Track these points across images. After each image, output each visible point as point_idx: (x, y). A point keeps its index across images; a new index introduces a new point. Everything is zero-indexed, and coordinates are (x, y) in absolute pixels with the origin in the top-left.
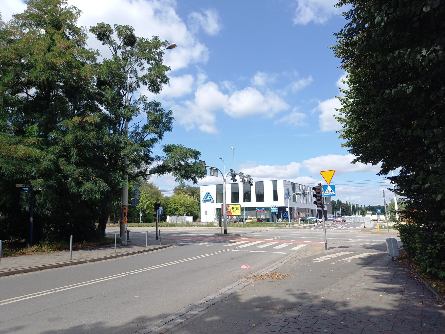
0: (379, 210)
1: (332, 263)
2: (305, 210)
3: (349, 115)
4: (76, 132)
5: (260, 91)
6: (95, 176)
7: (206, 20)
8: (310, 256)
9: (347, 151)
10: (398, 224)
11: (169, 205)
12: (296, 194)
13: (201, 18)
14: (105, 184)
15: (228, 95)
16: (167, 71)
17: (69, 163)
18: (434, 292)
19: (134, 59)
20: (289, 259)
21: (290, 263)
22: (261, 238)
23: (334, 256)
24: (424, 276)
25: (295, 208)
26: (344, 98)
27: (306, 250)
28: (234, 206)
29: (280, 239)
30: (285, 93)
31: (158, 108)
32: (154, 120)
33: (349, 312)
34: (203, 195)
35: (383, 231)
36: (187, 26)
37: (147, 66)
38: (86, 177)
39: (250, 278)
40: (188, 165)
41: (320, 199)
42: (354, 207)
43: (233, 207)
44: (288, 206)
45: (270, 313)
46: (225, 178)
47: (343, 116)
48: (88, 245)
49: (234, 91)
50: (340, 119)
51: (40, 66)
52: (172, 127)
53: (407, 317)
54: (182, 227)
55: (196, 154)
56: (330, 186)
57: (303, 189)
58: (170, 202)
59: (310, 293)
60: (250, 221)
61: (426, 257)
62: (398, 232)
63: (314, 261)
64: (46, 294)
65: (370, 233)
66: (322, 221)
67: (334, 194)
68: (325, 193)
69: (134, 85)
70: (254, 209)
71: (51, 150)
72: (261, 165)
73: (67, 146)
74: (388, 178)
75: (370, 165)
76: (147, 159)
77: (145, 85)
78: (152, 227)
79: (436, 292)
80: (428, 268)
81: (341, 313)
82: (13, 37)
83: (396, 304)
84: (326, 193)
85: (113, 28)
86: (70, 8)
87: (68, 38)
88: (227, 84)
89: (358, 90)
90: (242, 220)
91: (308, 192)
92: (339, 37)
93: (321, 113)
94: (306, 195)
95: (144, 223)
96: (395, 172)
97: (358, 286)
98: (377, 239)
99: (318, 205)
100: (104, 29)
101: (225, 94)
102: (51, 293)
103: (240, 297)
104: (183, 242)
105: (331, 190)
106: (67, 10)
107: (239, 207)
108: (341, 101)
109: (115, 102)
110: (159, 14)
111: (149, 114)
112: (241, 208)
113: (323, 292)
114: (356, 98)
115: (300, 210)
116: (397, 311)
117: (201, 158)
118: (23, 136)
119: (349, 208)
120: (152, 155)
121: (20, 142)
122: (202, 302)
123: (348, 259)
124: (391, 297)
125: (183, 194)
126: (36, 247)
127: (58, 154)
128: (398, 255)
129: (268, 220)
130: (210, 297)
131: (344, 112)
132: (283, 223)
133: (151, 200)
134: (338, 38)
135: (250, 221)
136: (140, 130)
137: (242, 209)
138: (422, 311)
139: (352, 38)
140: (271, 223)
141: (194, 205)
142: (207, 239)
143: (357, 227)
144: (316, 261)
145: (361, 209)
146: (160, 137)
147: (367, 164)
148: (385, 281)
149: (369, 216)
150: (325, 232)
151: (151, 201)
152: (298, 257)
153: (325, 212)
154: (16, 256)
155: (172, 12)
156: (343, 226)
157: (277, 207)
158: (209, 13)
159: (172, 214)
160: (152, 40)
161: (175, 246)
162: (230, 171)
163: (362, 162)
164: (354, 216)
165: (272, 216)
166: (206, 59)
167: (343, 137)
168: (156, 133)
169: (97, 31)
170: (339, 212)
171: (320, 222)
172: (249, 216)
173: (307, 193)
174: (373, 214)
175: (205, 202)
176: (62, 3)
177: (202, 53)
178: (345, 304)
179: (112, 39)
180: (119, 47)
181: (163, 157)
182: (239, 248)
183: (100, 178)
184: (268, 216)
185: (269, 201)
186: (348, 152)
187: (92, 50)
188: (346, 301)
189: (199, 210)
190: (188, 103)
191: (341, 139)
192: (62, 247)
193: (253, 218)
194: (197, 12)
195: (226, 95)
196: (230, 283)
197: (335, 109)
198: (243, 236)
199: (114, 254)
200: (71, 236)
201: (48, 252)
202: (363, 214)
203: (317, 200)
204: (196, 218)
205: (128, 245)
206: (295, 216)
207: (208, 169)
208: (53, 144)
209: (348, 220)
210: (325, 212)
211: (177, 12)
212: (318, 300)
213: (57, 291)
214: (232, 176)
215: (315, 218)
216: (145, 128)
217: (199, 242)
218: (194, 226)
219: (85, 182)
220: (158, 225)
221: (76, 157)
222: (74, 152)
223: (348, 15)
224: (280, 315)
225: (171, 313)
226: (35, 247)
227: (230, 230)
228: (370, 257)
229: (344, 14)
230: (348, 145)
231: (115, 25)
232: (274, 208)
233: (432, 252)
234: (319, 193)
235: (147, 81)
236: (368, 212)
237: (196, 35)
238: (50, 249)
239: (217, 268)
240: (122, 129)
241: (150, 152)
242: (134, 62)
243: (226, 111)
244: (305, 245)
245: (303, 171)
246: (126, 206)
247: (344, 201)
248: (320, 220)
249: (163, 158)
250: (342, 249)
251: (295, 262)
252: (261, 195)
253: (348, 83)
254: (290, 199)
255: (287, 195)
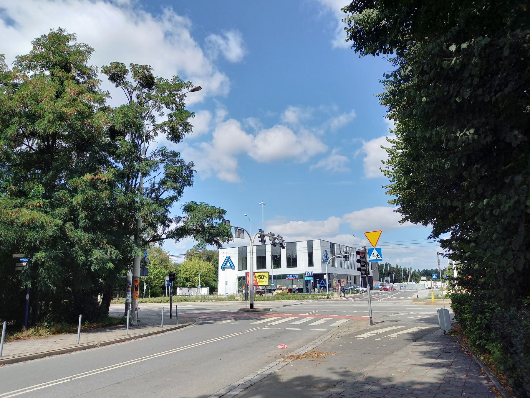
0: (434, 276)
1: (377, 339)
2: (347, 277)
3: (397, 168)
4: (87, 192)
5: (292, 129)
6: (105, 242)
7: (227, 44)
8: (352, 332)
9: (394, 211)
10: (450, 292)
11: (179, 273)
12: (336, 257)
13: (221, 41)
14: (117, 251)
15: (253, 134)
16: (190, 117)
17: (77, 228)
18: (480, 365)
19: (151, 103)
20: (329, 337)
21: (331, 341)
22: (294, 313)
23: (380, 331)
24: (474, 350)
25: (335, 275)
26: (392, 148)
27: (349, 326)
28: (261, 274)
29: (317, 313)
30: (322, 132)
31: (177, 159)
32: (172, 174)
33: (393, 386)
34: (221, 261)
35: (439, 301)
36: (204, 52)
37: (166, 111)
38: (95, 244)
39: (288, 357)
40: (212, 227)
41: (365, 265)
42: (405, 272)
43: (259, 275)
44: (327, 273)
45: (313, 391)
46: (253, 240)
47: (390, 170)
48: (91, 327)
49: (260, 130)
50: (387, 173)
51: (49, 116)
52: (193, 182)
53: (450, 389)
54: (197, 301)
55: (221, 213)
56: (377, 249)
57: (344, 251)
58: (180, 270)
59: (354, 370)
60: (280, 292)
61: (476, 328)
62: (449, 301)
63: (358, 338)
64: (68, 380)
65: (423, 304)
66: (367, 291)
67: (380, 259)
68: (370, 257)
69: (151, 133)
70: (284, 277)
71: (56, 213)
72: (293, 221)
73: (75, 208)
74: (438, 241)
75: (420, 224)
76: (165, 221)
77: (163, 133)
78: (159, 302)
79: (482, 364)
80: (478, 340)
81: (385, 388)
82: (16, 81)
83: (442, 377)
84: (372, 258)
85: (128, 67)
86: (80, 45)
87: (78, 82)
88: (251, 122)
89: (407, 140)
90: (269, 291)
91: (351, 255)
92: (386, 85)
93: (366, 155)
94: (348, 258)
95: (150, 298)
96: (446, 236)
97: (404, 361)
98: (432, 311)
99: (362, 272)
100: (118, 69)
101: (249, 134)
102: (73, 379)
103: (280, 377)
104: (203, 321)
105: (377, 254)
106: (77, 48)
107: (267, 275)
108: (389, 152)
109: (131, 155)
110: (170, 37)
111: (166, 167)
112: (269, 276)
113: (367, 369)
114: (404, 148)
115: (340, 277)
116: (441, 384)
117: (226, 217)
118: (26, 198)
119: (399, 273)
120: (171, 216)
121: (22, 205)
122: (241, 382)
123: (395, 335)
124: (437, 372)
125: (197, 260)
126: (32, 330)
127: (64, 217)
128: (450, 328)
129: (301, 290)
130: (248, 378)
131: (391, 165)
132: (320, 293)
133: (158, 268)
134: (384, 86)
135: (280, 292)
136: (156, 186)
137: (271, 277)
138: (465, 382)
139: (400, 85)
140: (306, 295)
141: (210, 273)
142: (231, 316)
143: (409, 297)
144: (360, 338)
145: (414, 274)
146: (180, 193)
147: (417, 224)
148: (434, 356)
149: (424, 283)
150: (370, 303)
151: (159, 269)
152: (339, 334)
153: (371, 278)
154: (11, 342)
155: (186, 35)
156: (392, 295)
157: (312, 273)
158: (230, 35)
159: (184, 286)
160: (172, 80)
161: (195, 325)
162: (258, 232)
163: (412, 221)
164: (406, 283)
165: (306, 285)
166: (226, 91)
167: (390, 193)
168: (175, 189)
169: (110, 71)
170: (388, 278)
171: (365, 292)
172: (278, 286)
173: (349, 256)
174: (428, 280)
175: (224, 268)
176: (70, 39)
177: (222, 84)
178: (389, 379)
179: (127, 81)
180: (134, 89)
181: (184, 217)
182: (270, 326)
183: (111, 245)
184: (301, 285)
185: (302, 267)
186: (395, 212)
187: (101, 91)
188: (391, 376)
189: (216, 280)
190: (204, 145)
191: (388, 195)
192: (63, 329)
193: (283, 288)
194: (217, 35)
195: (251, 135)
196: (267, 363)
197: (382, 161)
198: (273, 311)
199: (126, 336)
200: (80, 315)
201: (47, 336)
202: (416, 280)
203: (361, 266)
204: (213, 289)
205: (138, 325)
206: (335, 285)
207: (233, 231)
208: (58, 205)
209: (398, 289)
210: (371, 278)
211: (192, 35)
212: (362, 377)
213: (78, 377)
214: (261, 238)
215: (358, 286)
216: (163, 183)
217: (221, 319)
218: (212, 300)
219: (95, 251)
220: (173, 299)
221: (85, 220)
222: (82, 215)
223: (396, 61)
224: (324, 393)
225: (212, 393)
226: (31, 330)
227: (257, 305)
228: (421, 331)
229: (391, 60)
230: (396, 202)
231: (130, 64)
232: (308, 275)
233: (481, 323)
234: (363, 258)
235: (166, 128)
236: (422, 278)
237: (214, 62)
238: (49, 333)
239: (249, 348)
240: (135, 185)
241: (168, 212)
242: (152, 106)
243: (251, 154)
244: (346, 320)
245: (344, 228)
246: (138, 278)
247: (393, 265)
248: (365, 289)
249: (183, 219)
250: (389, 324)
251: (336, 339)
252: (293, 258)
253: (396, 132)
254: (328, 263)
255: (325, 259)
